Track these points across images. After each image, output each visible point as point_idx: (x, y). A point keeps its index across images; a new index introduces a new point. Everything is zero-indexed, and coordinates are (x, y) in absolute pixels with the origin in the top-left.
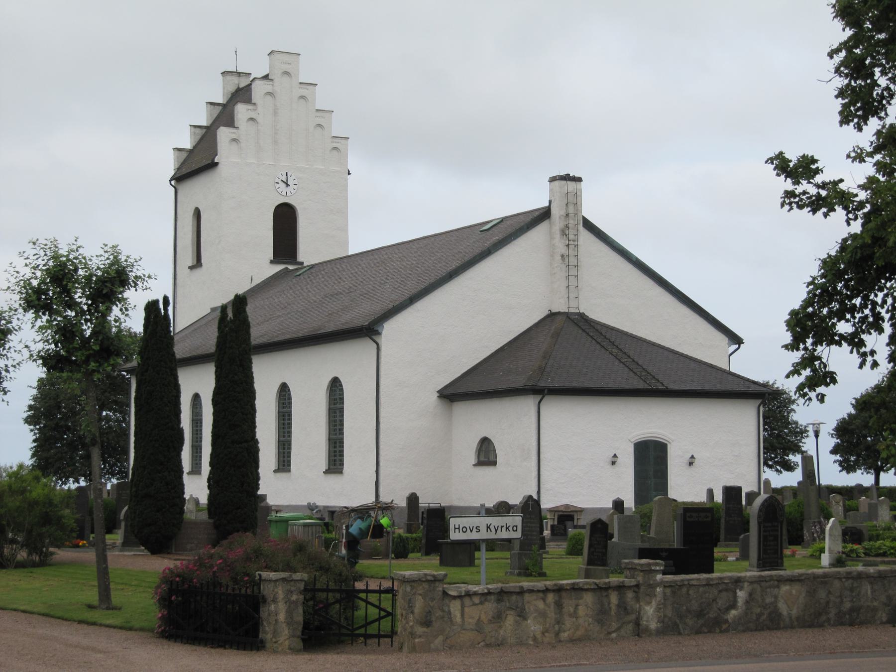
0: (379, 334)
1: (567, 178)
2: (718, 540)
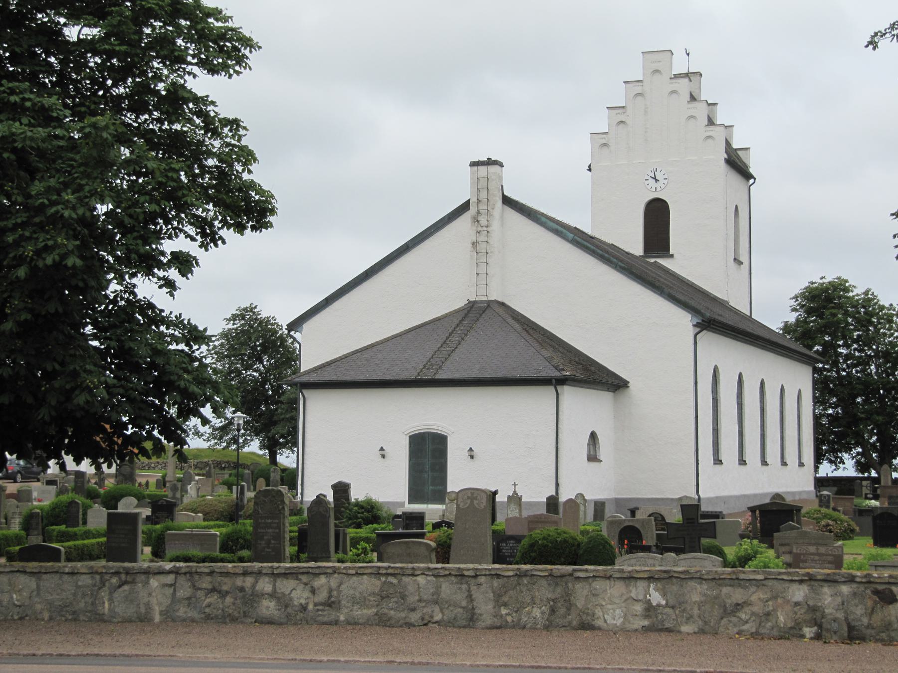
0: (694, 326)
1: (490, 162)
2: (615, 557)
